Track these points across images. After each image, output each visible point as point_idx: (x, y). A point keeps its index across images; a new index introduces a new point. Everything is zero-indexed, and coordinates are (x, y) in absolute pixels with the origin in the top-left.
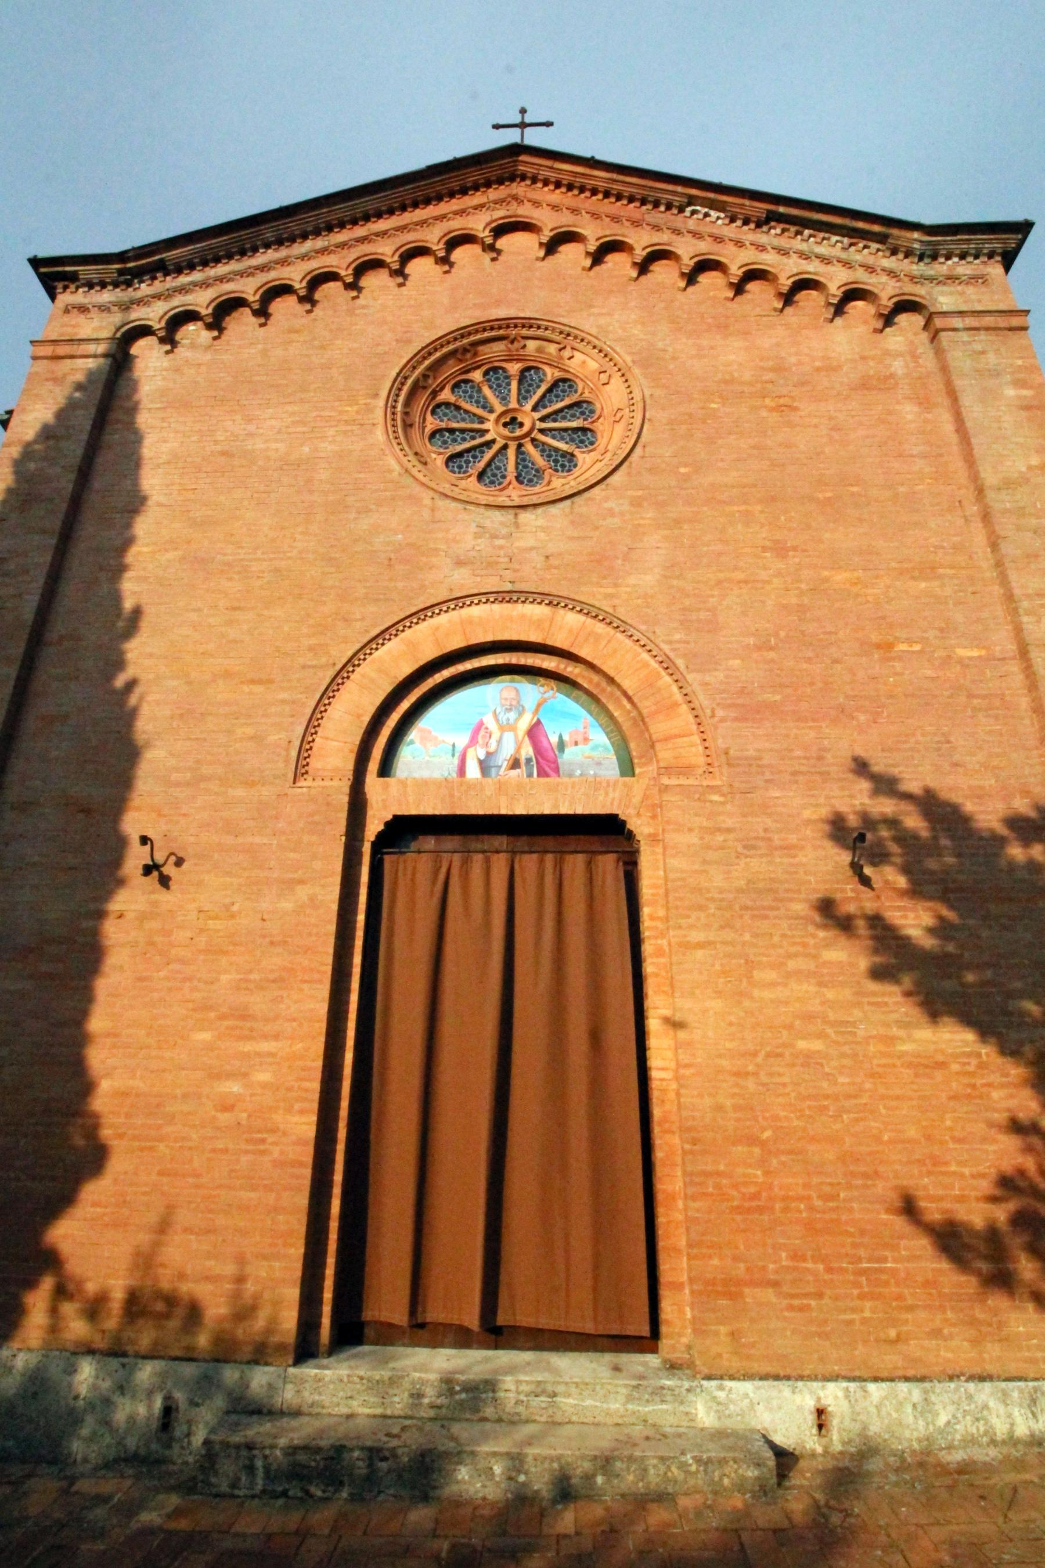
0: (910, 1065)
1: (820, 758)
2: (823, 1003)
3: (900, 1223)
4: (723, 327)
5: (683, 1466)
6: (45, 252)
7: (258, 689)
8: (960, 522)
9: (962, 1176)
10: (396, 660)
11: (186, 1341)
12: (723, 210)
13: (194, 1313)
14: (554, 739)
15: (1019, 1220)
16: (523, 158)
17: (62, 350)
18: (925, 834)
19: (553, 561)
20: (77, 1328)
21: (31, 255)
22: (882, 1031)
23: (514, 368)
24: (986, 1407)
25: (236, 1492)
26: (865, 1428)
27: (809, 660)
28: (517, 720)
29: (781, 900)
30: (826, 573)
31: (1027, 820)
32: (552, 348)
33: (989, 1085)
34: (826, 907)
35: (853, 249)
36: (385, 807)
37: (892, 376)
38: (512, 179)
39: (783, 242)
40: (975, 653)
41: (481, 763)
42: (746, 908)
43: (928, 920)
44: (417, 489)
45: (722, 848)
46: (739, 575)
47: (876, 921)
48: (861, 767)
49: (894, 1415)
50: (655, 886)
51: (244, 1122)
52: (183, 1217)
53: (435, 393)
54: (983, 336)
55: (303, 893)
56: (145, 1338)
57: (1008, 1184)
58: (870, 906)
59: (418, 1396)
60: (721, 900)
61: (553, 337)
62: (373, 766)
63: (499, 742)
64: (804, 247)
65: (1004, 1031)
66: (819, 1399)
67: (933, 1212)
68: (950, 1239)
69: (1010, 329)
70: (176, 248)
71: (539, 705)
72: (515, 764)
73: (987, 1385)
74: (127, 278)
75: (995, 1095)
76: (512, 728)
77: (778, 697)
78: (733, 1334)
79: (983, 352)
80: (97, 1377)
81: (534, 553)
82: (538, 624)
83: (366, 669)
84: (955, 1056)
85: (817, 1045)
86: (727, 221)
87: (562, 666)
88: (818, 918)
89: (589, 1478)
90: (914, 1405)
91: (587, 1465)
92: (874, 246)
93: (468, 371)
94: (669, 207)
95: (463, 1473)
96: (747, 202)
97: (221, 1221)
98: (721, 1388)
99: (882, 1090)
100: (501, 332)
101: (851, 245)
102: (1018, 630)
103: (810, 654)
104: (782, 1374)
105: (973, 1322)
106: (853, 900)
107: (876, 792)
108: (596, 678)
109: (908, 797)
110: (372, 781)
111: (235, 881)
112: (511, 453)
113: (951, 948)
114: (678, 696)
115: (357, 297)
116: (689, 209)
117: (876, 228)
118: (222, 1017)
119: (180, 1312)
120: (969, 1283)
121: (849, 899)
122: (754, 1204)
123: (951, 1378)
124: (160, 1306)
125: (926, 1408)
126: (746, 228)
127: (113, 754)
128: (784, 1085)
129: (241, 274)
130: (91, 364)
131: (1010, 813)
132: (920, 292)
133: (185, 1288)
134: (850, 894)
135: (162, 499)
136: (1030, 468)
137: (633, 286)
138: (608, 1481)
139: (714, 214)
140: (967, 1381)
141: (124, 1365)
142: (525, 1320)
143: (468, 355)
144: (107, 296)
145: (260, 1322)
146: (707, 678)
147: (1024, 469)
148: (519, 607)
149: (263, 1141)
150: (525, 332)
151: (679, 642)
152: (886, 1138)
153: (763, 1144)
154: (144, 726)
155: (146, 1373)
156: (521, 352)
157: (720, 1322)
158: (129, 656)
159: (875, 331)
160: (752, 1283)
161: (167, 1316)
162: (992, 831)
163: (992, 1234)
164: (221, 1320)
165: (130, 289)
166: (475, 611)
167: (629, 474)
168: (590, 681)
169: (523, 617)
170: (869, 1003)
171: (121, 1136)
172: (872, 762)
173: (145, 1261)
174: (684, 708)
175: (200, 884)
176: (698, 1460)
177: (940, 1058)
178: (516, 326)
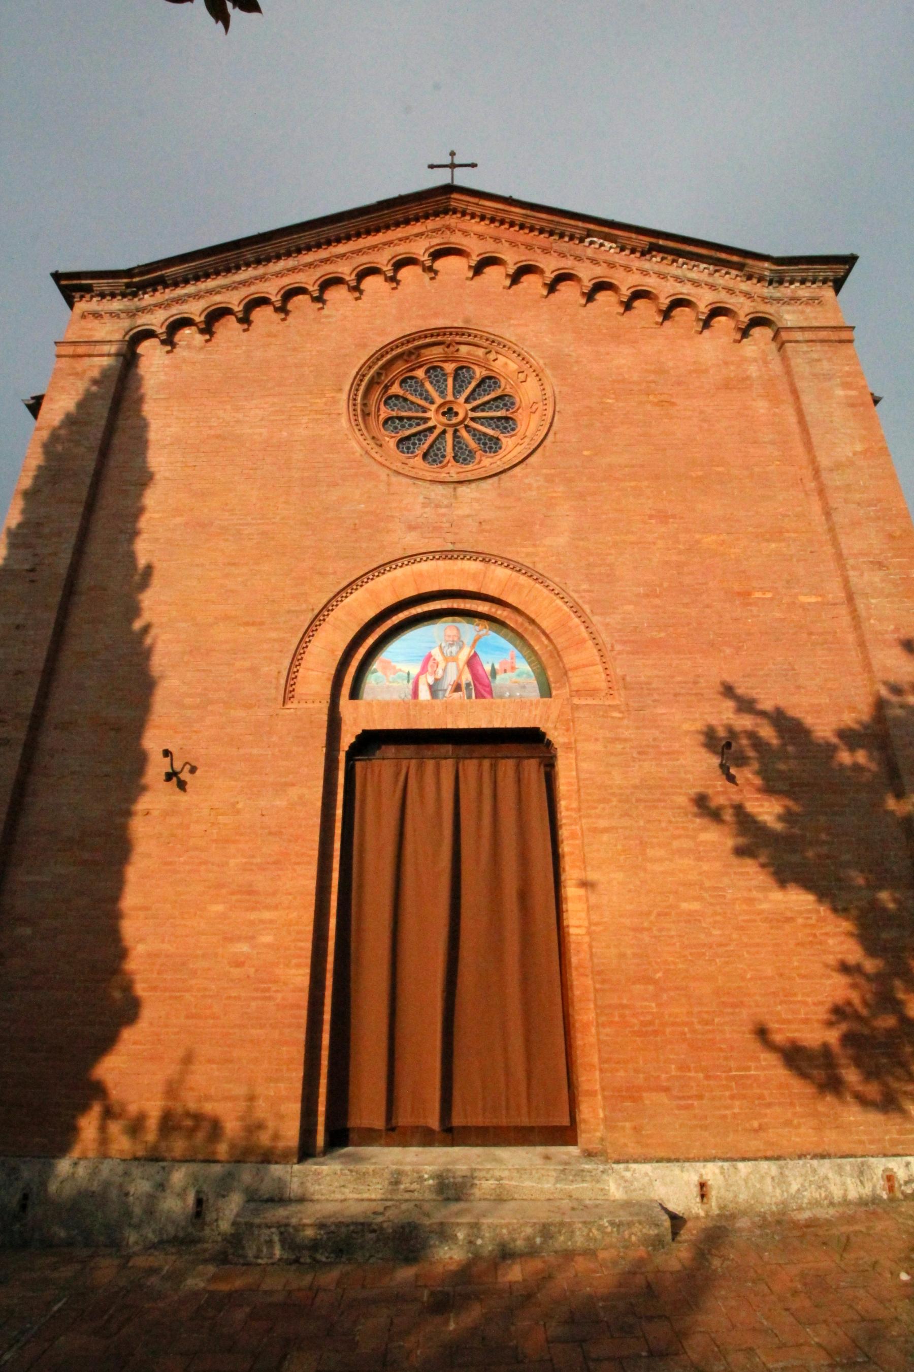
0: (766, 920)
2: (700, 874)
3: (755, 1046)
4: (616, 337)
5: (601, 1228)
6: (62, 269)
7: (253, 630)
8: (802, 496)
9: (805, 1003)
10: (362, 606)
13: (215, 1128)
14: (488, 668)
15: (848, 1039)
16: (454, 196)
17: (81, 350)
18: (775, 742)
19: (486, 527)
20: (122, 1144)
21: (53, 270)
22: (745, 894)
24: (826, 1178)
27: (686, 605)
28: (458, 653)
30: (698, 536)
32: (480, 352)
33: (826, 934)
34: (701, 802)
35: (717, 274)
37: (748, 378)
38: (446, 212)
40: (813, 599)
42: (638, 800)
46: (632, 538)
48: (728, 691)
49: (758, 1186)
53: (387, 388)
54: (818, 347)
55: (294, 793)
56: (179, 1145)
57: (839, 1012)
58: (737, 798)
60: (621, 795)
62: (346, 690)
63: (445, 670)
65: (837, 892)
66: (701, 1176)
68: (795, 1057)
71: (475, 641)
75: (831, 941)
76: (454, 659)
77: (662, 635)
81: (470, 520)
82: (474, 576)
83: (338, 614)
84: (800, 913)
85: (695, 906)
86: (618, 250)
88: (695, 810)
90: (773, 1178)
91: (529, 1230)
92: (734, 272)
94: (572, 238)
96: (634, 236)
97: (236, 1053)
98: (627, 1169)
99: (745, 940)
100: (440, 338)
101: (716, 271)
104: (682, 1157)
106: (722, 794)
108: (520, 619)
109: (763, 714)
110: (345, 704)
113: (796, 831)
115: (322, 308)
116: (588, 240)
117: (735, 259)
122: (650, 1029)
123: (800, 1157)
124: (189, 1123)
128: (672, 937)
129: (227, 288)
130: (105, 361)
131: (842, 725)
132: (769, 310)
133: (209, 1108)
134: (720, 789)
135: (167, 474)
136: (855, 454)
139: (608, 244)
140: (812, 1159)
143: (413, 357)
144: (117, 305)
148: (459, 562)
150: (458, 339)
151: (585, 591)
152: (749, 976)
153: (655, 982)
154: (158, 663)
155: (179, 1176)
160: (650, 1089)
165: (136, 299)
166: (425, 566)
169: (462, 570)
173: (172, 1090)
174: (590, 643)
176: (612, 1223)
177: (789, 914)
178: (451, 334)
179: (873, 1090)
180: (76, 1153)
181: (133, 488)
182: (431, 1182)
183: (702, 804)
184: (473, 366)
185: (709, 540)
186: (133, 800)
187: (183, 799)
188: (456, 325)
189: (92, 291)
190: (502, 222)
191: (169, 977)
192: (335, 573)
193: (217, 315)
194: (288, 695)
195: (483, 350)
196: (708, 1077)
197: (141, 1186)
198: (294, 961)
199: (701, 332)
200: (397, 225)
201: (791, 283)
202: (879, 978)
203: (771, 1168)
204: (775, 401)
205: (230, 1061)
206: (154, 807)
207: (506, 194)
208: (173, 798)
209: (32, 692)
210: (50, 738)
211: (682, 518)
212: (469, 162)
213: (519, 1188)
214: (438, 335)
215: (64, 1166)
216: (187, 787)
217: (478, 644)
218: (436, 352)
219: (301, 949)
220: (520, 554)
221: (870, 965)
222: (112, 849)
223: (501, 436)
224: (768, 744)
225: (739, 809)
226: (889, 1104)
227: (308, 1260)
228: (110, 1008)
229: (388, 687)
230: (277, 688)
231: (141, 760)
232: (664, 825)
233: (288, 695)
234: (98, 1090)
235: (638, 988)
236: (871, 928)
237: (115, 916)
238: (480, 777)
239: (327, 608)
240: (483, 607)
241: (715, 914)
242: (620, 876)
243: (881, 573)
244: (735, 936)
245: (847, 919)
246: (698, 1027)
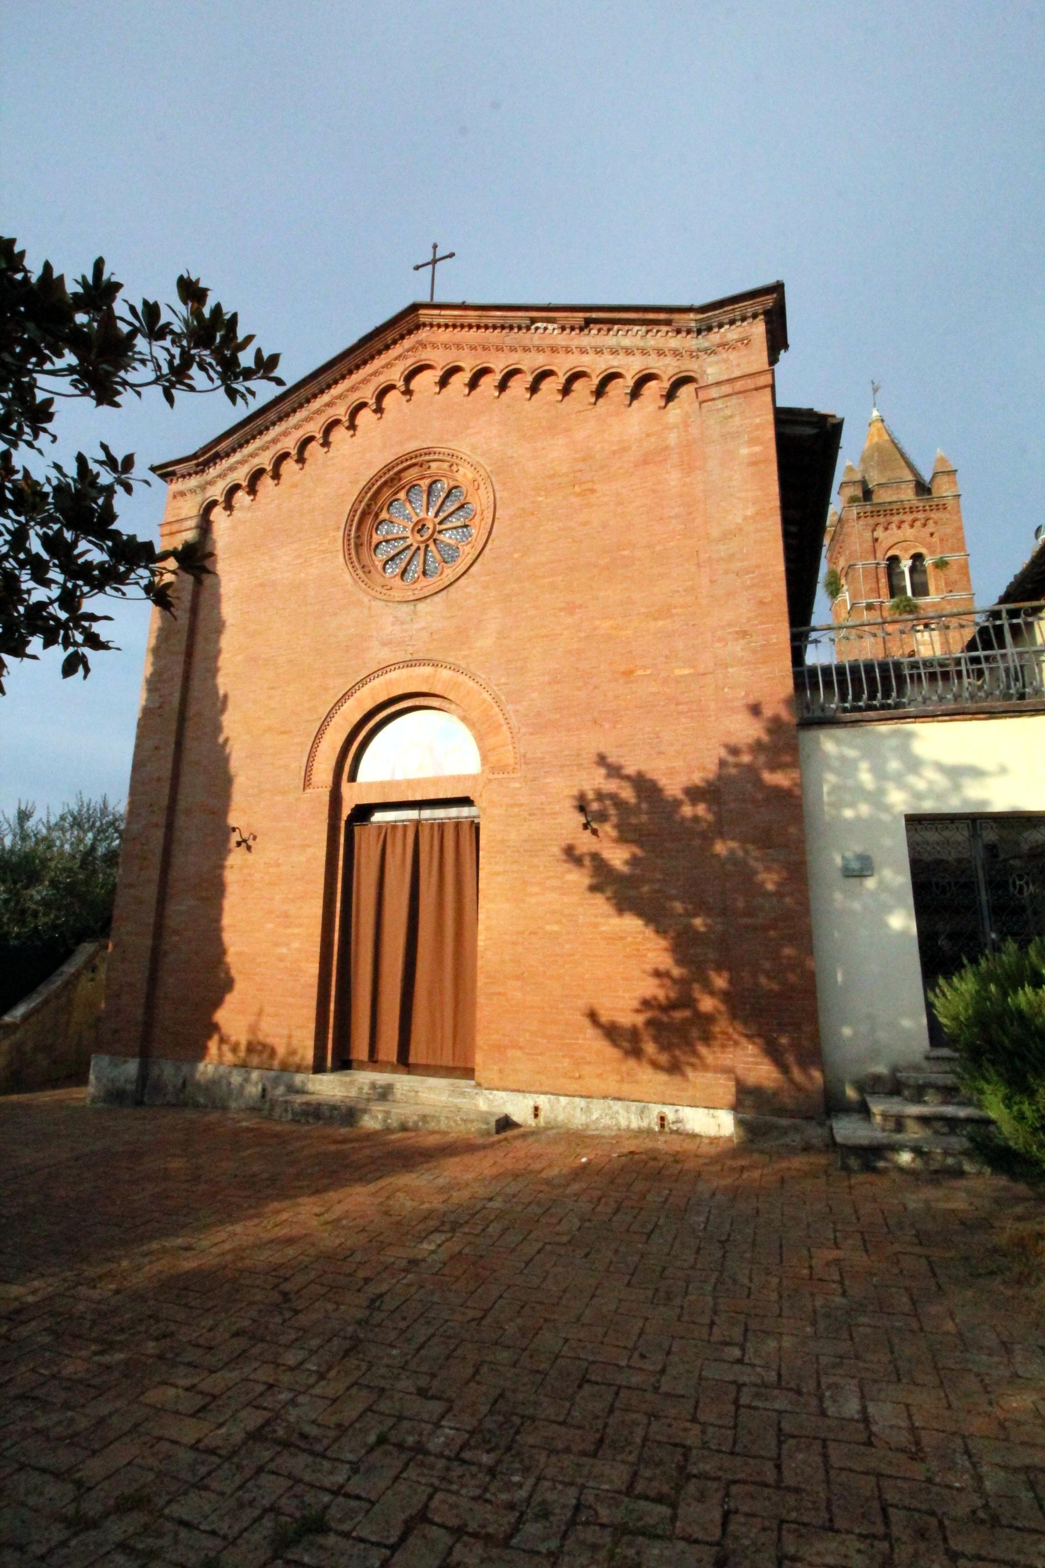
3: (586, 1022)
4: (552, 429)
5: (455, 1121)
7: (285, 737)
8: (694, 569)
13: (273, 1052)
15: (649, 1023)
16: (422, 312)
17: (175, 527)
18: (633, 801)
19: (435, 637)
20: (229, 1057)
22: (593, 920)
23: (424, 483)
27: (579, 689)
30: (597, 623)
31: (697, 788)
32: (446, 465)
40: (686, 671)
46: (544, 631)
47: (595, 857)
48: (602, 760)
52: (268, 1009)
53: (377, 515)
54: (734, 401)
55: (310, 851)
56: (255, 1060)
57: (646, 1004)
59: (361, 1089)
68: (611, 1032)
69: (756, 389)
75: (650, 955)
78: (501, 1071)
79: (731, 417)
82: (426, 680)
83: (337, 719)
88: (564, 857)
91: (416, 1118)
92: (664, 329)
94: (520, 328)
95: (366, 1117)
97: (282, 1011)
101: (648, 332)
103: (580, 684)
105: (618, 1073)
106: (586, 843)
107: (609, 776)
109: (628, 778)
110: (345, 787)
113: (638, 871)
114: (502, 721)
117: (662, 316)
123: (605, 1097)
124: (259, 1048)
125: (587, 1111)
131: (689, 784)
132: (691, 366)
133: (269, 1040)
136: (745, 518)
139: (550, 326)
142: (422, 1061)
144: (193, 482)
146: (518, 707)
147: (740, 521)
148: (416, 669)
150: (427, 458)
154: (235, 764)
155: (255, 1075)
159: (660, 408)
166: (393, 675)
172: (608, 755)
173: (253, 1029)
174: (505, 728)
179: (664, 1058)
180: (207, 1060)
183: (570, 854)
186: (224, 859)
187: (251, 857)
193: (257, 475)
194: (307, 783)
197: (236, 1079)
199: (630, 405)
200: (379, 353)
201: (720, 326)
202: (683, 983)
203: (582, 1103)
209: (166, 790)
210: (181, 820)
213: (427, 1098)
215: (201, 1066)
221: (676, 972)
222: (213, 890)
224: (627, 803)
226: (674, 1068)
228: (217, 984)
233: (307, 783)
234: (215, 1028)
236: (684, 945)
238: (432, 836)
239: (329, 716)
241: (569, 933)
243: (742, 642)
245: (665, 938)
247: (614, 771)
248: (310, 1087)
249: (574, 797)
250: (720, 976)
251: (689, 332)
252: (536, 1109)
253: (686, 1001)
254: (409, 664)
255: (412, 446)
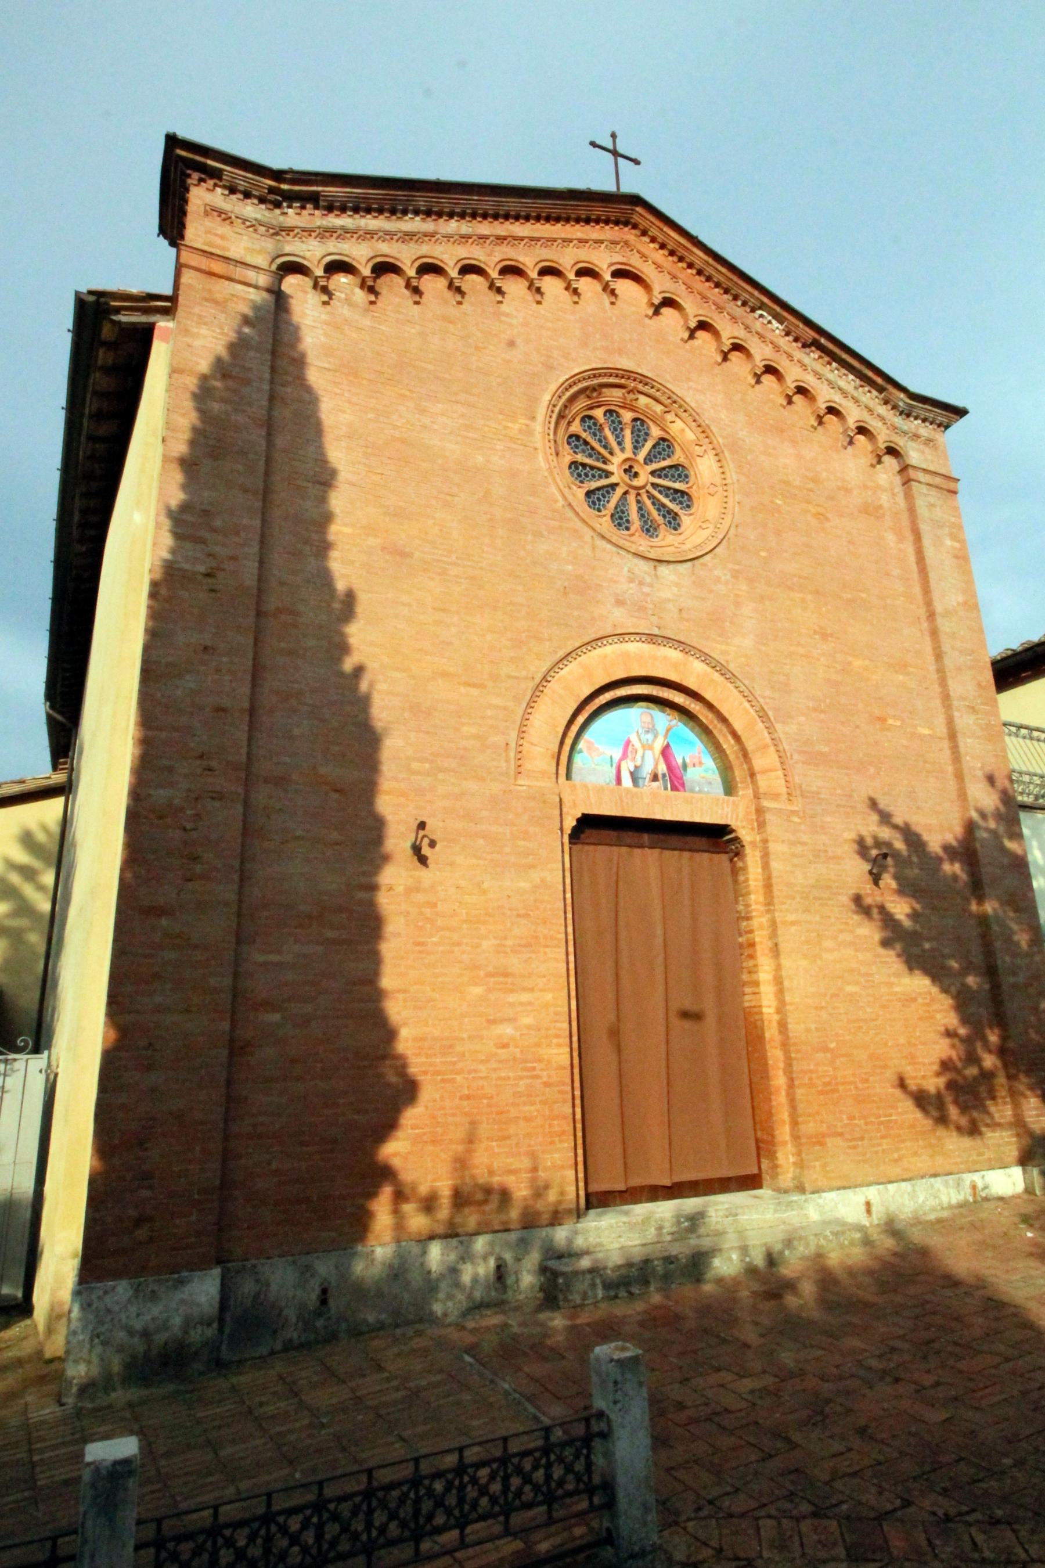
0: (899, 1000)
1: (851, 796)
3: (898, 1092)
5: (825, 1237)
6: (184, 133)
7: (475, 692)
11: (503, 1217)
12: (781, 323)
13: (505, 1196)
14: (680, 761)
15: (951, 1085)
16: (638, 209)
17: (218, 267)
18: (905, 853)
19: (685, 615)
20: (417, 1222)
21: (171, 131)
24: (939, 1190)
25: (586, 1302)
26: (887, 1209)
28: (654, 741)
29: (835, 894)
31: (953, 848)
32: (659, 408)
35: (861, 389)
36: (575, 805)
37: (880, 507)
38: (626, 223)
39: (818, 366)
40: (926, 732)
41: (632, 774)
42: (816, 898)
43: (907, 910)
44: (579, 524)
45: (802, 856)
46: (801, 650)
50: (756, 880)
51: (518, 1056)
54: (933, 492)
55: (536, 876)
56: (471, 1219)
57: (946, 1065)
58: (879, 899)
59: (660, 1228)
61: (663, 399)
63: (643, 757)
64: (831, 376)
67: (912, 1085)
68: (921, 1099)
70: (332, 185)
71: (668, 731)
72: (655, 778)
73: (939, 1179)
74: (275, 199)
75: (939, 1016)
76: (650, 747)
77: (826, 749)
80: (443, 1255)
82: (675, 666)
84: (920, 994)
86: (783, 333)
87: (688, 703)
89: (781, 1253)
92: (875, 393)
93: (591, 408)
94: (744, 304)
96: (801, 325)
98: (820, 1198)
100: (623, 381)
101: (862, 386)
102: (950, 722)
105: (931, 1146)
106: (872, 896)
108: (711, 715)
109: (896, 827)
111: (481, 862)
112: (619, 491)
113: (918, 927)
114: (768, 740)
115: (501, 302)
116: (759, 312)
117: (879, 380)
118: (490, 975)
119: (495, 1199)
120: (928, 1123)
121: (868, 895)
122: (829, 1088)
123: (922, 1177)
124: (479, 1196)
125: (913, 1195)
126: (794, 344)
127: (354, 739)
130: (253, 295)
132: (900, 442)
133: (496, 1180)
134: (869, 891)
135: (350, 477)
137: (717, 370)
138: (791, 1252)
141: (461, 1242)
143: (595, 394)
145: (552, 1196)
146: (787, 729)
148: (662, 648)
149: (534, 1069)
150: (640, 387)
154: (382, 711)
155: (480, 1244)
156: (634, 403)
157: (816, 1160)
158: (353, 641)
160: (829, 1135)
161: (486, 1202)
162: (936, 853)
163: (939, 1096)
164: (525, 1199)
165: (278, 211)
166: (633, 647)
167: (728, 548)
168: (707, 717)
169: (665, 658)
170: (881, 962)
171: (425, 1073)
173: (461, 1163)
174: (772, 749)
175: (452, 864)
176: (832, 1233)
177: (914, 995)
178: (635, 380)
179: (964, 1121)
181: (310, 485)
182: (686, 1224)
184: (651, 423)
185: (858, 663)
187: (422, 873)
188: (640, 371)
189: (220, 179)
190: (681, 259)
191: (438, 1060)
192: (550, 640)
193: (384, 268)
195: (662, 407)
196: (866, 1124)
198: (555, 1041)
201: (916, 418)
204: (901, 539)
205: (508, 1137)
206: (396, 884)
207: (693, 232)
208: (417, 873)
211: (838, 638)
212: (633, 156)
214: (623, 377)
216: (429, 862)
217: (670, 734)
218: (614, 395)
219: (560, 1029)
220: (715, 649)
221: (962, 1031)
223: (681, 512)
225: (882, 908)
226: (973, 1130)
227: (625, 1295)
228: (389, 1094)
229: (594, 769)
230: (507, 761)
231: (376, 827)
232: (833, 920)
234: (385, 1173)
235: (820, 1056)
237: (377, 995)
240: (679, 698)
242: (804, 963)
244: (881, 1013)
246: (860, 1085)
247: (885, 818)
248: (580, 1242)
249: (855, 841)
250: (993, 1032)
251: (894, 407)
252: (868, 1204)
253: (971, 1058)
254: (651, 638)
255: (624, 363)
